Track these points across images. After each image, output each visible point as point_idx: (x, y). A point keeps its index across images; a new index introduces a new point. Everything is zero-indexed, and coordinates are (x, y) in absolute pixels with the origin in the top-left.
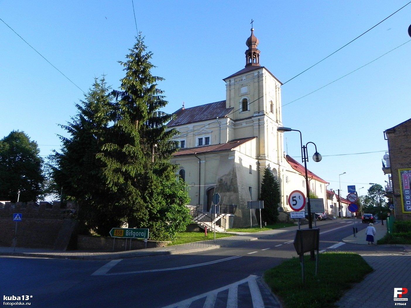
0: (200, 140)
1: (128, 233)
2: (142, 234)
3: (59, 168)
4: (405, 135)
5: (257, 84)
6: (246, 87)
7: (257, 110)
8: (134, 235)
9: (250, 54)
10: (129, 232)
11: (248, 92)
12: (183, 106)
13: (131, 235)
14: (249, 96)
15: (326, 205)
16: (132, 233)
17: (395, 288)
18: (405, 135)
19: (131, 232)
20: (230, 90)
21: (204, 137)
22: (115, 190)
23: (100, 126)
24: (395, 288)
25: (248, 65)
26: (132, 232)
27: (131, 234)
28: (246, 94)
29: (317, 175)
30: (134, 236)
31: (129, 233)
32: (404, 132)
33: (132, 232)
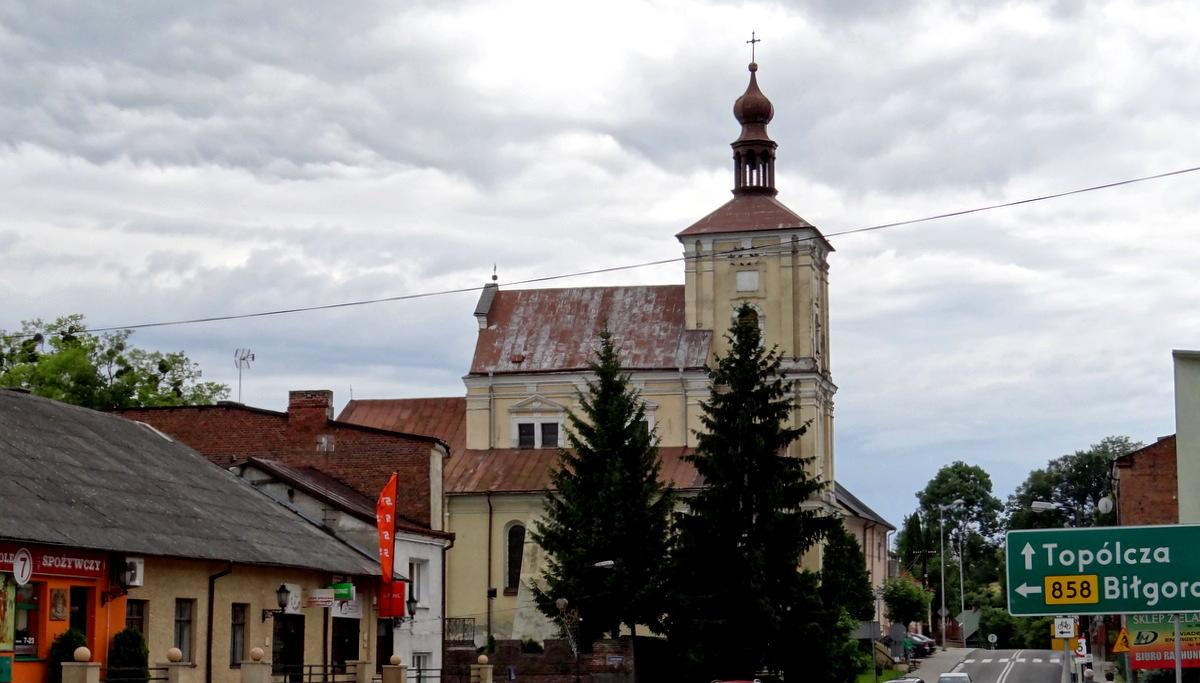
0: (526, 431)
1: (1115, 587)
2: (1170, 590)
3: (131, 563)
4: (1150, 475)
5: (789, 272)
6: (754, 275)
7: (789, 353)
8: (1155, 595)
9: (755, 153)
10: (1121, 583)
11: (758, 291)
12: (495, 278)
13: (1136, 596)
14: (761, 303)
15: (78, 579)
16: (1141, 588)
17: (1046, 579)
18: (1150, 475)
19: (1130, 582)
20: (699, 274)
21: (537, 421)
22: (309, 602)
23: (540, 647)
24: (1046, 579)
25: (741, 190)
26: (1136, 582)
27: (1131, 592)
28: (754, 295)
29: (885, 519)
30: (1152, 599)
31: (1120, 587)
32: (1150, 467)
33: (1136, 582)
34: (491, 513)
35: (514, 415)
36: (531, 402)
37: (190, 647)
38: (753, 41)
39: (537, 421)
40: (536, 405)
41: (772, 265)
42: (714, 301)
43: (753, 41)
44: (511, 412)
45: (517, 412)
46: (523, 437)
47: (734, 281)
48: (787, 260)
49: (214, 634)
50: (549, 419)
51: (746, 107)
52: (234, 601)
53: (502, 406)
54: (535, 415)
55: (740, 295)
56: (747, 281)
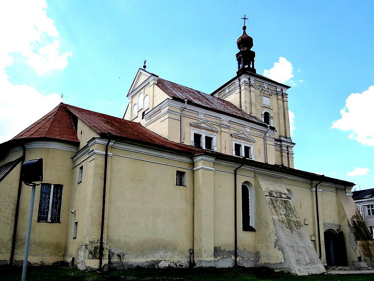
0: (197, 137)
21: (204, 134)
37: (284, 115)
39: (204, 134)
41: (274, 97)
43: (245, 19)
44: (191, 125)
47: (262, 100)
48: (280, 97)
50: (210, 134)
53: (186, 121)
54: (203, 130)
56: (266, 101)
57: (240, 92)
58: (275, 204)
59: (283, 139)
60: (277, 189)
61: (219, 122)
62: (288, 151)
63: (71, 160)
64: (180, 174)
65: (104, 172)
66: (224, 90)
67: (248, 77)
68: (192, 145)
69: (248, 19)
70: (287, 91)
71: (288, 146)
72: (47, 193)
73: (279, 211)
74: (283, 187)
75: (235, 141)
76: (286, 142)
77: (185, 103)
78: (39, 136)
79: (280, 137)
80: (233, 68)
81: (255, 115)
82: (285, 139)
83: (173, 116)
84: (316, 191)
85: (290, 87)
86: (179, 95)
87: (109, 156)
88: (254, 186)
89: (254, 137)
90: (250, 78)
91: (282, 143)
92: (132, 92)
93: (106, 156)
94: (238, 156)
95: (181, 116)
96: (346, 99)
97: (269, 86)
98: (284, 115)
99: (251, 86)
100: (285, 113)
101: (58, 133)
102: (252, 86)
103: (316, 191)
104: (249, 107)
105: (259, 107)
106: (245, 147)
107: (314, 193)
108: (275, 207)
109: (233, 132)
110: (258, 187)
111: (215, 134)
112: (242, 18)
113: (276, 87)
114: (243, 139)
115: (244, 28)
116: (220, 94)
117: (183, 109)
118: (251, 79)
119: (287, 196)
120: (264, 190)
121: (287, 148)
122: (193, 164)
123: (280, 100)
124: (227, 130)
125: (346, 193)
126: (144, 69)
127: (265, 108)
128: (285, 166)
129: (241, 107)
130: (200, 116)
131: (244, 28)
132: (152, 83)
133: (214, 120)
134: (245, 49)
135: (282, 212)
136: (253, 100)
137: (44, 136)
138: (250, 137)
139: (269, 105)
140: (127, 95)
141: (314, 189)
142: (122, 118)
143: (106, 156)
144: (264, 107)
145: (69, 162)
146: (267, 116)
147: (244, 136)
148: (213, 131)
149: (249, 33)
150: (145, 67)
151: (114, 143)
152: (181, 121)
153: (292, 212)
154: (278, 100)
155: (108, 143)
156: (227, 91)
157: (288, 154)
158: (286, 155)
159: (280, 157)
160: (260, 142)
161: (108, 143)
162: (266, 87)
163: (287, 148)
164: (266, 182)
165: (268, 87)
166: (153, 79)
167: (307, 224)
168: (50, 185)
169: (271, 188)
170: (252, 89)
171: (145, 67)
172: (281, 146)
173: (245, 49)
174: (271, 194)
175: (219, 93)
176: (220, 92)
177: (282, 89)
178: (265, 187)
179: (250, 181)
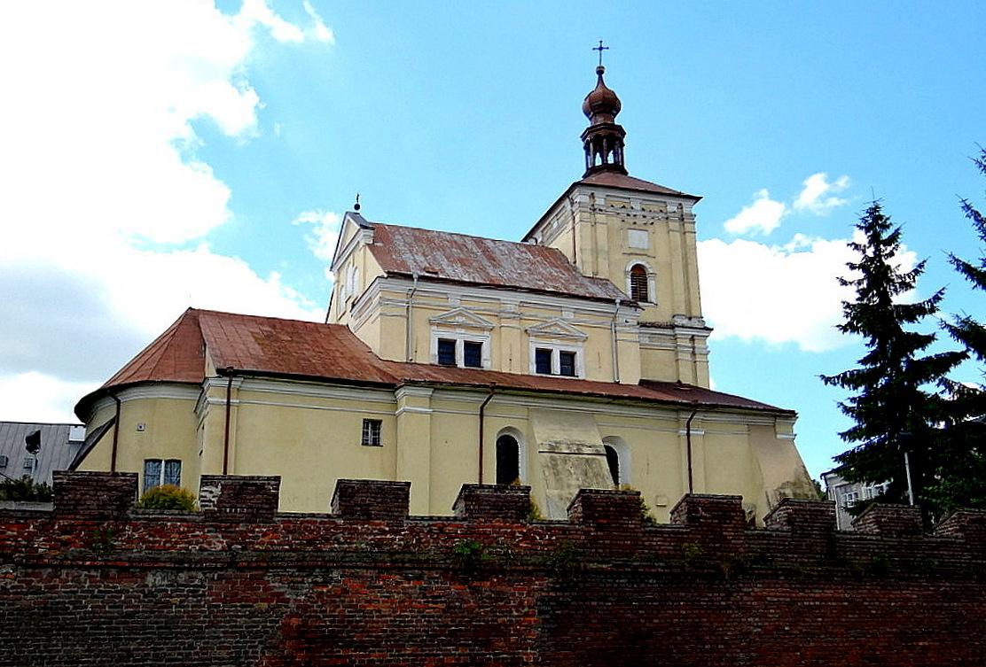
0: (446, 347)
11: (648, 250)
21: (460, 338)
34: (482, 416)
35: (434, 328)
36: (454, 316)
37: (686, 265)
38: (601, 49)
39: (460, 338)
40: (460, 319)
41: (660, 227)
42: (608, 252)
43: (601, 49)
44: (431, 323)
45: (438, 325)
46: (450, 351)
47: (626, 238)
48: (675, 225)
49: (119, 433)
50: (474, 337)
51: (606, 96)
52: (55, 469)
53: (420, 316)
54: (458, 330)
55: (632, 251)
56: (638, 239)
57: (574, 228)
58: (560, 467)
59: (679, 321)
60: (575, 438)
61: (496, 308)
62: (694, 348)
63: (194, 414)
64: (373, 426)
65: (224, 432)
66: (549, 223)
67: (590, 192)
68: (432, 362)
69: (594, 49)
70: (695, 209)
71: (693, 336)
72: (155, 476)
73: (565, 480)
74: (593, 432)
75: (535, 344)
76: (686, 327)
77: (413, 280)
78: (139, 380)
79: (674, 316)
80: (575, 164)
81: (608, 274)
82: (685, 322)
83: (389, 311)
84: (688, 435)
85: (700, 198)
86: (415, 262)
87: (682, 352)
88: (525, 434)
89: (587, 330)
90: (592, 194)
91: (677, 332)
92: (339, 258)
93: (228, 404)
94: (546, 373)
95: (408, 309)
96: (707, 239)
97: (645, 202)
98: (686, 265)
99: (597, 211)
100: (689, 261)
101: (171, 371)
102: (600, 210)
103: (688, 435)
104: (590, 260)
105: (617, 256)
106: (563, 354)
107: (682, 441)
108: (557, 474)
109: (528, 325)
110: (531, 437)
111: (486, 333)
112: (594, 49)
113: (665, 202)
114: (558, 336)
115: (600, 72)
116: (545, 232)
117: (413, 292)
118: (595, 195)
119: (597, 450)
120: (539, 442)
121: (692, 339)
122: (395, 403)
123: (673, 231)
124: (514, 323)
125: (776, 434)
126: (356, 211)
127: (634, 256)
128: (684, 383)
129: (575, 262)
130: (451, 302)
131: (600, 72)
132: (362, 244)
133: (476, 306)
134: (600, 120)
135: (574, 482)
136: (602, 242)
137: (146, 379)
138: (575, 330)
139: (646, 248)
140: (331, 268)
141: (681, 432)
142: (324, 322)
143: (228, 404)
144: (632, 254)
145: (190, 420)
146: (639, 274)
147: (559, 329)
148: (483, 329)
149: (610, 85)
150: (357, 207)
151: (242, 382)
152: (408, 319)
153: (600, 480)
154: (668, 232)
155: (230, 385)
156: (555, 225)
157: (694, 354)
158: (688, 357)
159: (674, 363)
160: (601, 338)
161: (230, 385)
162: (637, 207)
163: (692, 339)
164: (551, 426)
165: (643, 207)
166: (364, 235)
167: (665, 506)
168: (160, 461)
169: (560, 436)
170: (600, 217)
171: (357, 207)
172: (675, 337)
173: (600, 120)
174: (552, 450)
175: (542, 232)
176: (544, 229)
177: (680, 204)
178: (545, 436)
179: (517, 427)
